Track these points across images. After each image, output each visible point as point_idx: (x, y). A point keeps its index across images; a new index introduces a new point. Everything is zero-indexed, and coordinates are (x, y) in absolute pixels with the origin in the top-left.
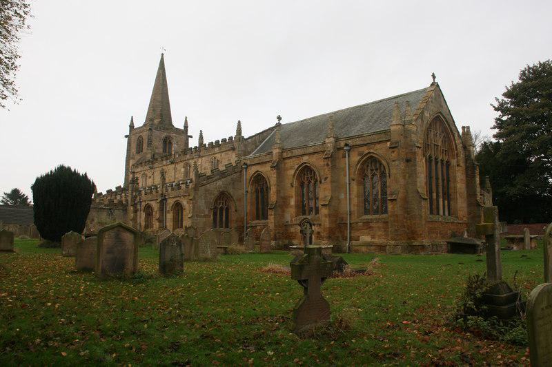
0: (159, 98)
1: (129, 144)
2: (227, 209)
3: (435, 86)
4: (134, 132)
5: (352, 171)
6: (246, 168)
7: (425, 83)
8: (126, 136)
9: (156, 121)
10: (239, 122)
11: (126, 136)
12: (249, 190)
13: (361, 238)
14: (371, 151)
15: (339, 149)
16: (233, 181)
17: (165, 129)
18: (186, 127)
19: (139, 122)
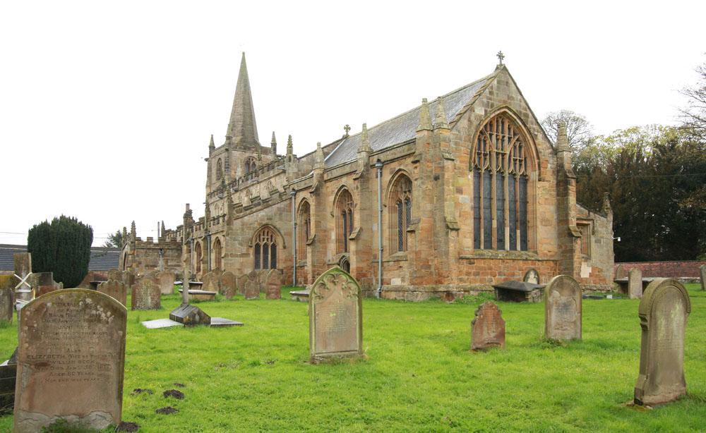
0: (240, 110)
1: (210, 169)
2: (274, 247)
3: (502, 70)
4: (214, 153)
5: (384, 192)
6: (295, 195)
7: (488, 69)
8: (206, 160)
9: (236, 139)
10: (290, 137)
11: (206, 160)
12: (298, 222)
13: (392, 280)
14: (402, 167)
15: (373, 166)
16: (281, 211)
17: (245, 149)
18: (274, 145)
19: (220, 141)
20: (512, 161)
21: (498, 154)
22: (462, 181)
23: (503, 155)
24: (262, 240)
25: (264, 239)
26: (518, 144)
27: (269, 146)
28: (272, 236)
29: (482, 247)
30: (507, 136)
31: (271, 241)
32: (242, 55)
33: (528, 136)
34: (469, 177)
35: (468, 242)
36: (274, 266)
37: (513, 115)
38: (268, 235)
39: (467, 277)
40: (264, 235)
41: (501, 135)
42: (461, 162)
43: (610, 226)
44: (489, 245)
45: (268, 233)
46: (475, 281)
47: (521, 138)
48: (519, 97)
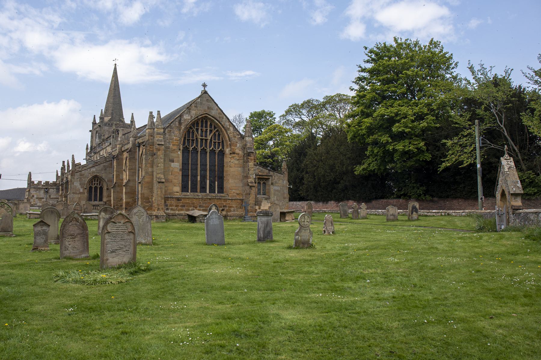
2: (101, 189)
8: (90, 131)
11: (90, 131)
20: (213, 143)
21: (202, 140)
22: (174, 155)
23: (206, 140)
24: (93, 184)
25: (95, 184)
26: (217, 134)
27: (129, 122)
28: (100, 182)
29: (190, 191)
30: (209, 129)
31: (100, 185)
32: (114, 66)
33: (223, 129)
34: (179, 153)
35: (177, 189)
36: (101, 200)
37: (212, 118)
38: (97, 181)
39: (176, 208)
40: (95, 181)
41: (204, 129)
42: (173, 145)
43: (286, 178)
44: (194, 190)
45: (97, 180)
46: (182, 210)
47: (219, 130)
48: (217, 107)
